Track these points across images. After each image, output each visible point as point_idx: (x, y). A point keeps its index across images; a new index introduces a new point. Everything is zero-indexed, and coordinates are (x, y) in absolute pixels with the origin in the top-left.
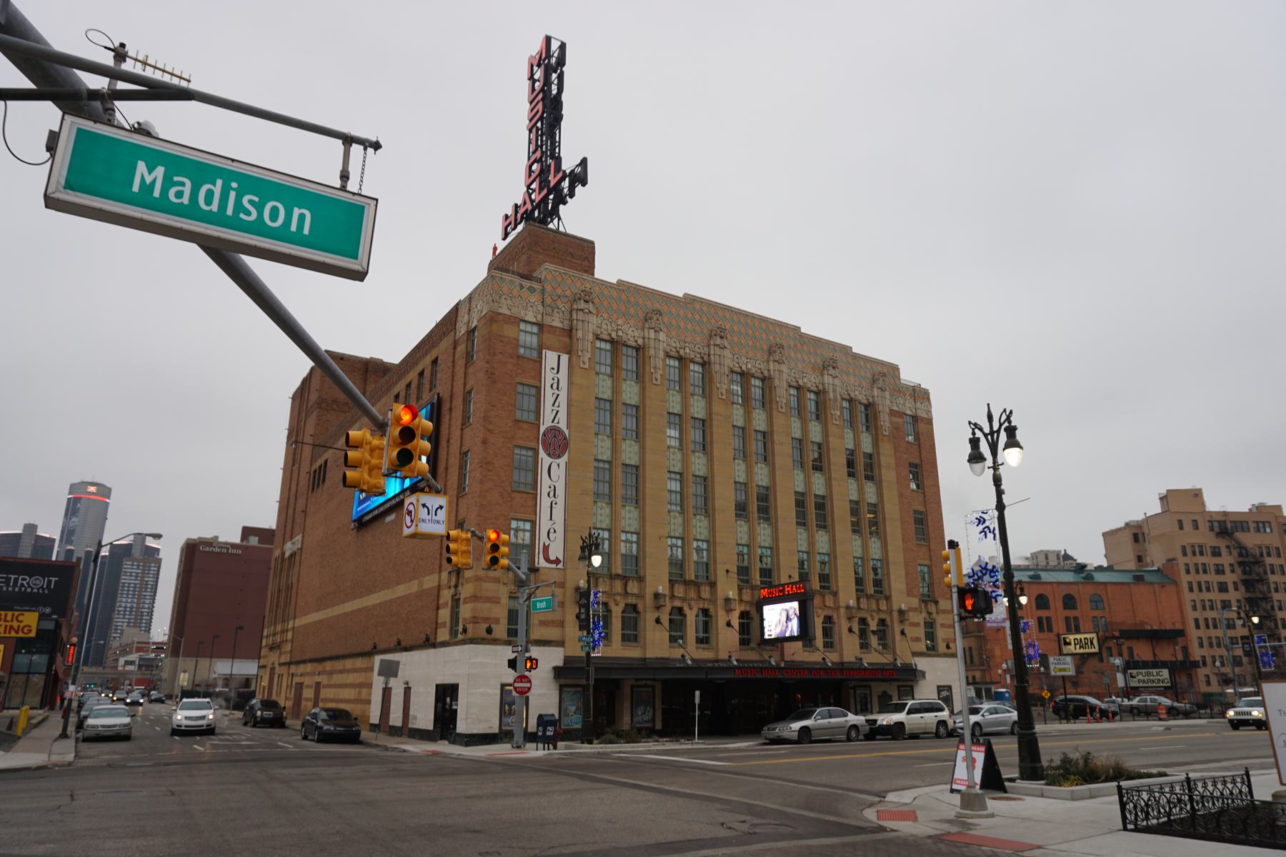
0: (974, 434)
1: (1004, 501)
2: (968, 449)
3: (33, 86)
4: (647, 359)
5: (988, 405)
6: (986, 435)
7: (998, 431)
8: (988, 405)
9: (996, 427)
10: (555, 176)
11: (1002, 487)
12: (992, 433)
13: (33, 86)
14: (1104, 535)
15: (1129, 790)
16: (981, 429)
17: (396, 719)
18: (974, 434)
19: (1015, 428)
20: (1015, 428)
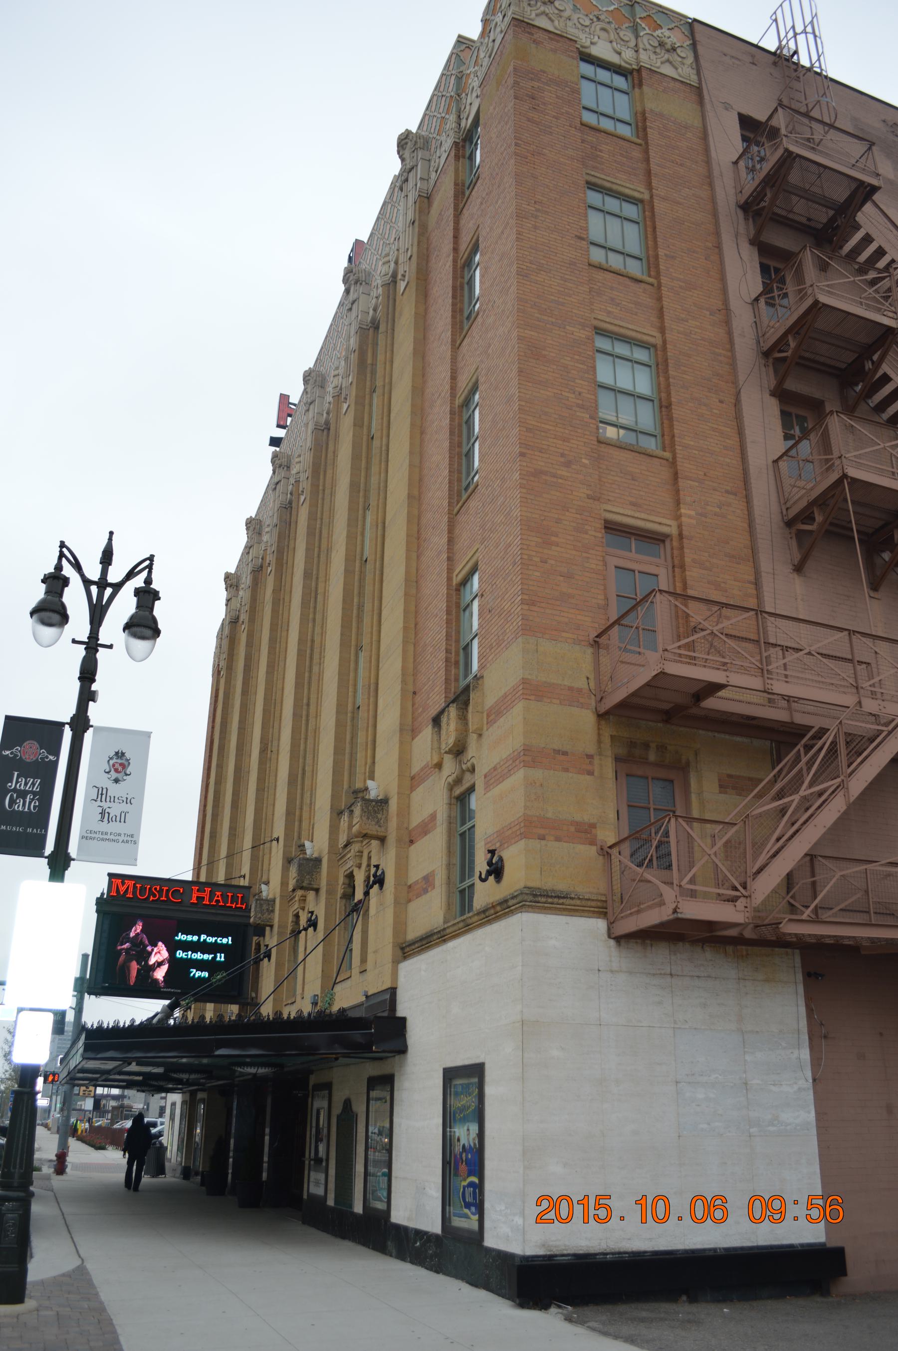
0: (59, 567)
1: (90, 713)
2: (39, 592)
3: (167, 1002)
4: (628, 535)
5: (111, 533)
6: (87, 583)
7: (117, 587)
8: (111, 533)
9: (114, 576)
10: (792, 801)
11: (94, 687)
12: (102, 584)
13: (167, 1002)
14: (8, 718)
15: (103, 1096)
16: (77, 566)
17: (431, 118)
18: (59, 567)
19: (156, 596)
20: (156, 596)
